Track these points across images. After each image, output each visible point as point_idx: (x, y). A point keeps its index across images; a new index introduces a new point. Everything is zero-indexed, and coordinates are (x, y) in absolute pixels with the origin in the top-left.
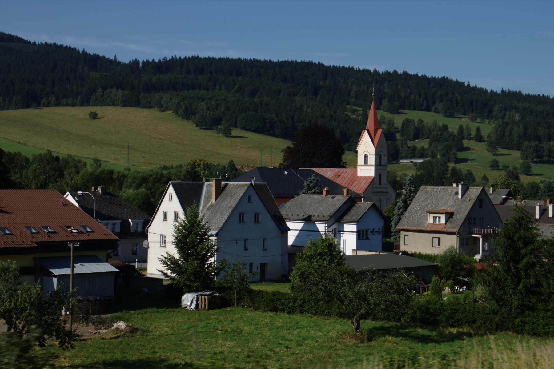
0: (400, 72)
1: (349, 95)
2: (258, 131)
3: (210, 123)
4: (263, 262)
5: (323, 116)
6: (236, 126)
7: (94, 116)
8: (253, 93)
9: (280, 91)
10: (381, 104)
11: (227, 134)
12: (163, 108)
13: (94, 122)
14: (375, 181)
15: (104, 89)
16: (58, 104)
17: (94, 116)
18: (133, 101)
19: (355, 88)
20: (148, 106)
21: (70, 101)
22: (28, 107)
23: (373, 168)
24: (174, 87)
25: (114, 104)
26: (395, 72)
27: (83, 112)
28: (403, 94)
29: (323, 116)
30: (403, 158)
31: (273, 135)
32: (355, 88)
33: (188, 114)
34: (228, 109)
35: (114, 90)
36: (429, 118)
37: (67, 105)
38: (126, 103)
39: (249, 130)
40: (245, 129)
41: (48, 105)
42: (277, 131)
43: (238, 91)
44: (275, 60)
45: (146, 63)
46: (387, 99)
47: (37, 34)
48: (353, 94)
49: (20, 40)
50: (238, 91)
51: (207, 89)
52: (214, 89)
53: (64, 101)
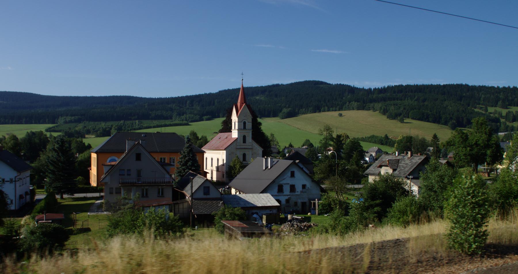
0: (511, 87)
1: (480, 99)
2: (419, 119)
3: (393, 117)
4: (296, 187)
5: (458, 111)
6: (408, 117)
7: (341, 115)
8: (424, 100)
9: (437, 99)
10: (497, 104)
11: (402, 121)
12: (374, 110)
13: (340, 118)
14: (238, 140)
15: (350, 102)
16: (329, 111)
17: (341, 115)
18: (362, 107)
19: (483, 96)
20: (369, 109)
21: (334, 109)
22: (315, 112)
23: (251, 131)
24: (384, 100)
25: (353, 109)
26: (509, 87)
27: (336, 113)
28: (510, 98)
29: (458, 111)
30: (501, 132)
31: (428, 121)
32: (483, 96)
33: (384, 112)
34: (405, 109)
35: (354, 102)
36: (392, 102)
37: (333, 111)
38: (358, 109)
39: (415, 119)
40: (413, 119)
41: (324, 111)
42: (431, 119)
43: (416, 100)
44: (442, 84)
45: (375, 89)
46: (501, 101)
47: (333, 80)
48: (482, 99)
49: (326, 83)
50: (416, 100)
51: (401, 100)
52: (405, 100)
53: (331, 109)
